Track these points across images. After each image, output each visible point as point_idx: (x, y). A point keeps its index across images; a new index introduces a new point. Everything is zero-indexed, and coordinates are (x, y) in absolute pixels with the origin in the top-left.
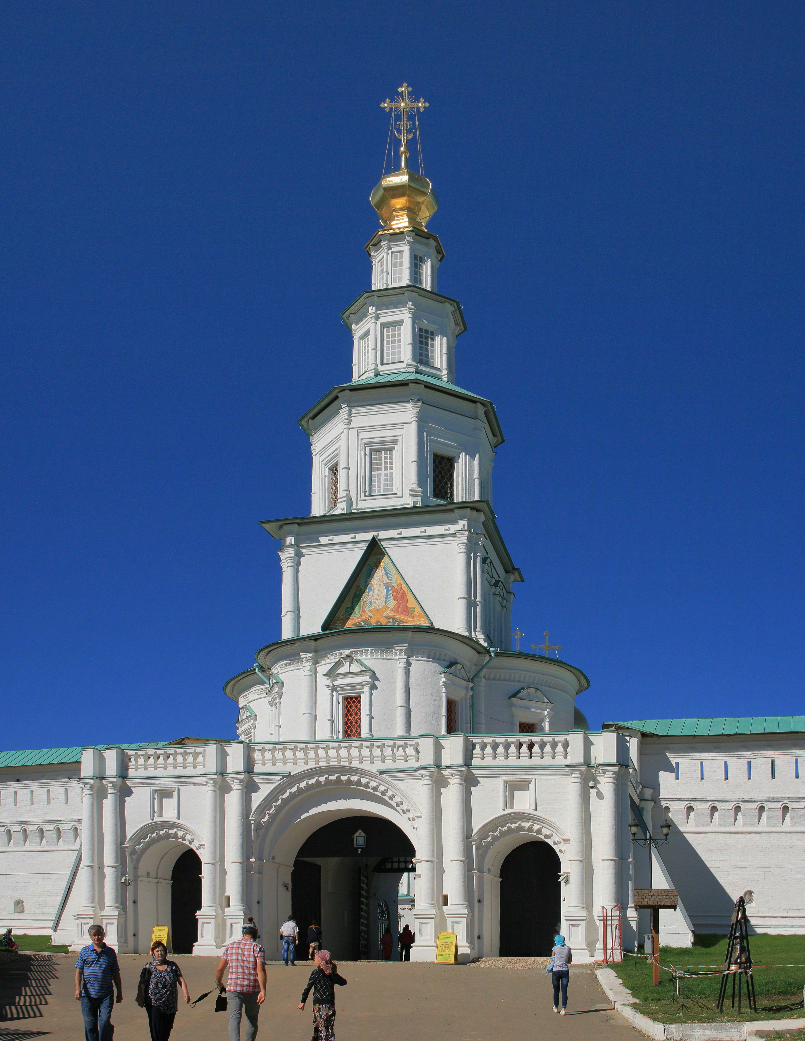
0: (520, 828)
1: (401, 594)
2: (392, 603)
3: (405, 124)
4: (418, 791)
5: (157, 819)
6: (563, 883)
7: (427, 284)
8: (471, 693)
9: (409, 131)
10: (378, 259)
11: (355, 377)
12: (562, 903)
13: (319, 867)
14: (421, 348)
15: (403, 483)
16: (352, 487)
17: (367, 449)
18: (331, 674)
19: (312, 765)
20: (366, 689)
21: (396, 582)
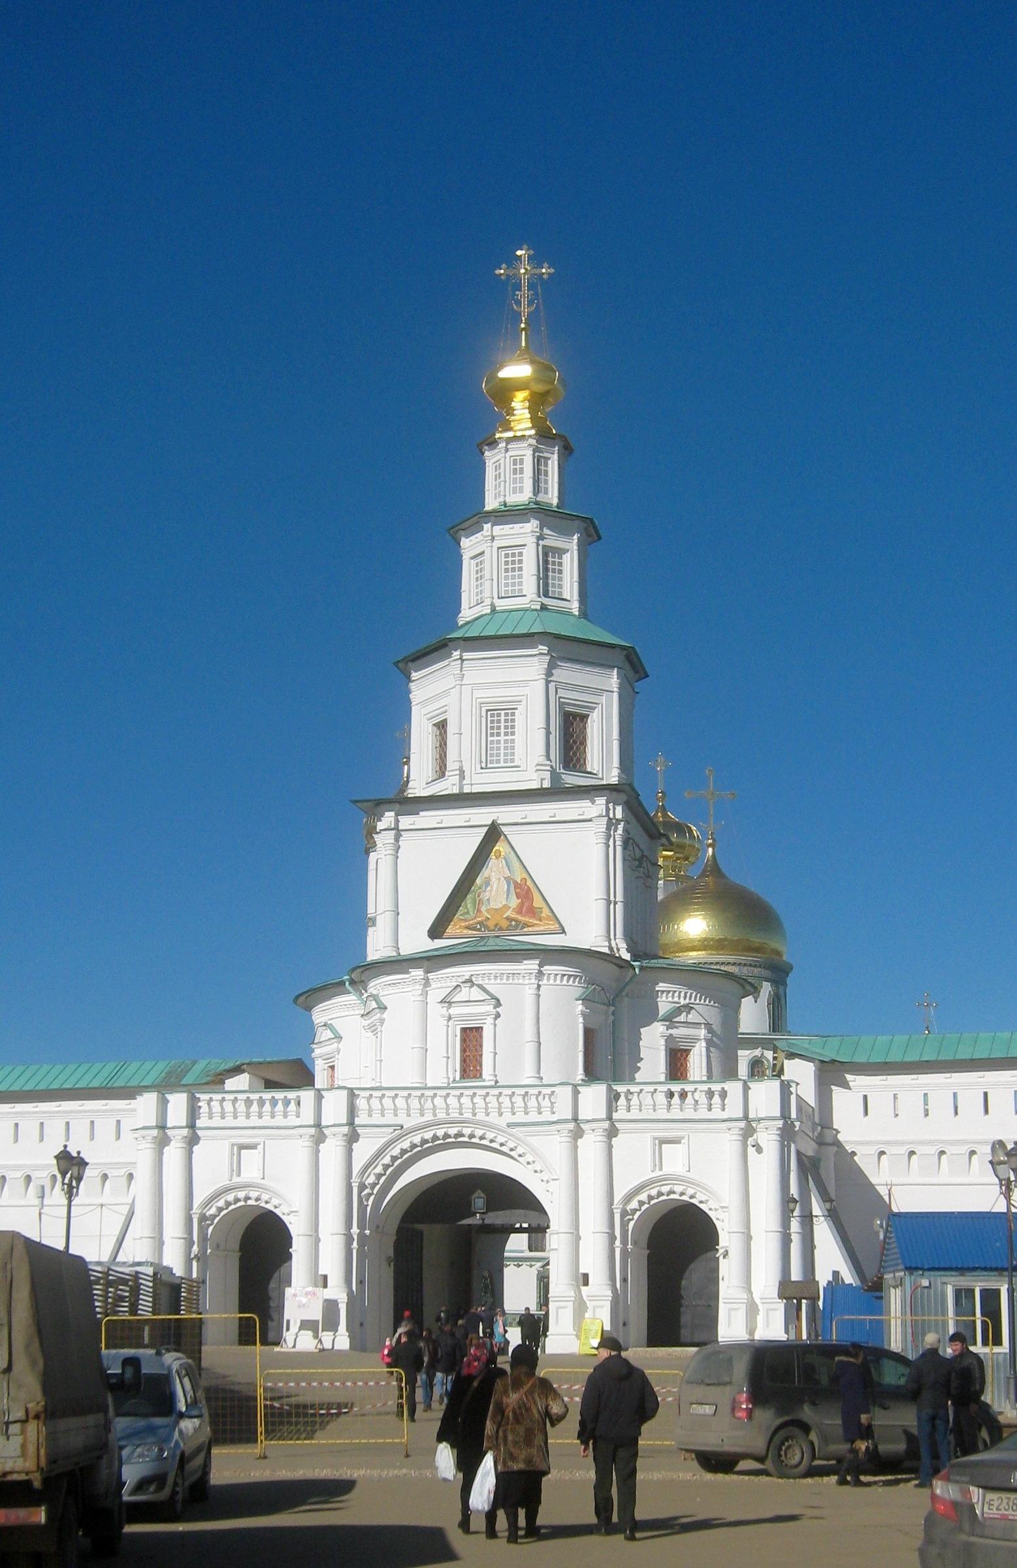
1: (525, 892)
2: (514, 902)
3: (524, 294)
4: (554, 1146)
5: (236, 1179)
7: (552, 496)
8: (612, 1018)
9: (530, 303)
10: (493, 461)
11: (466, 613)
12: (720, 1281)
13: (421, 1233)
15: (530, 758)
16: (465, 757)
17: (484, 710)
18: (447, 1002)
19: (428, 1117)
20: (490, 1020)
21: (519, 876)
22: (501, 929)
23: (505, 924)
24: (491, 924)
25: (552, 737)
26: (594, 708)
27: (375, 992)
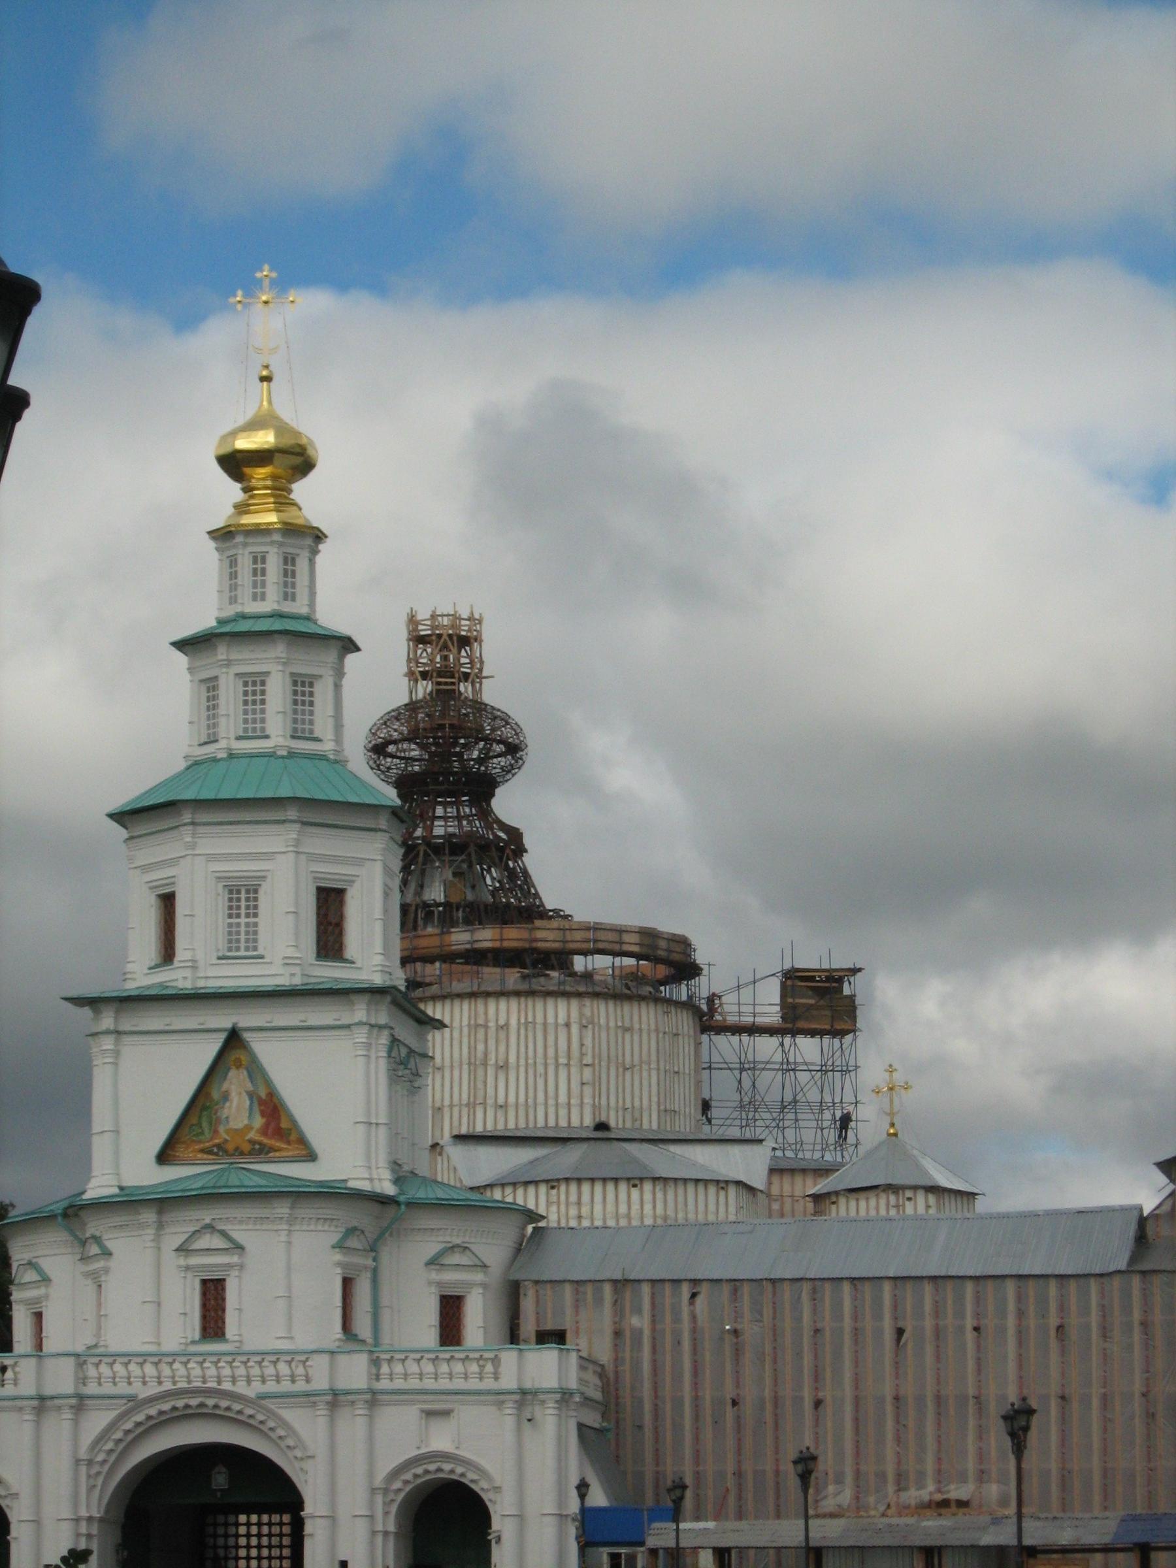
0: (439, 1470)
1: (272, 1108)
2: (259, 1122)
6: (493, 1542)
14: (286, 584)
15: (283, 948)
18: (182, 1250)
19: (168, 1386)
22: (242, 1154)
23: (246, 1147)
24: (230, 1147)
25: (312, 1022)
26: (353, 882)
27: (98, 1234)
